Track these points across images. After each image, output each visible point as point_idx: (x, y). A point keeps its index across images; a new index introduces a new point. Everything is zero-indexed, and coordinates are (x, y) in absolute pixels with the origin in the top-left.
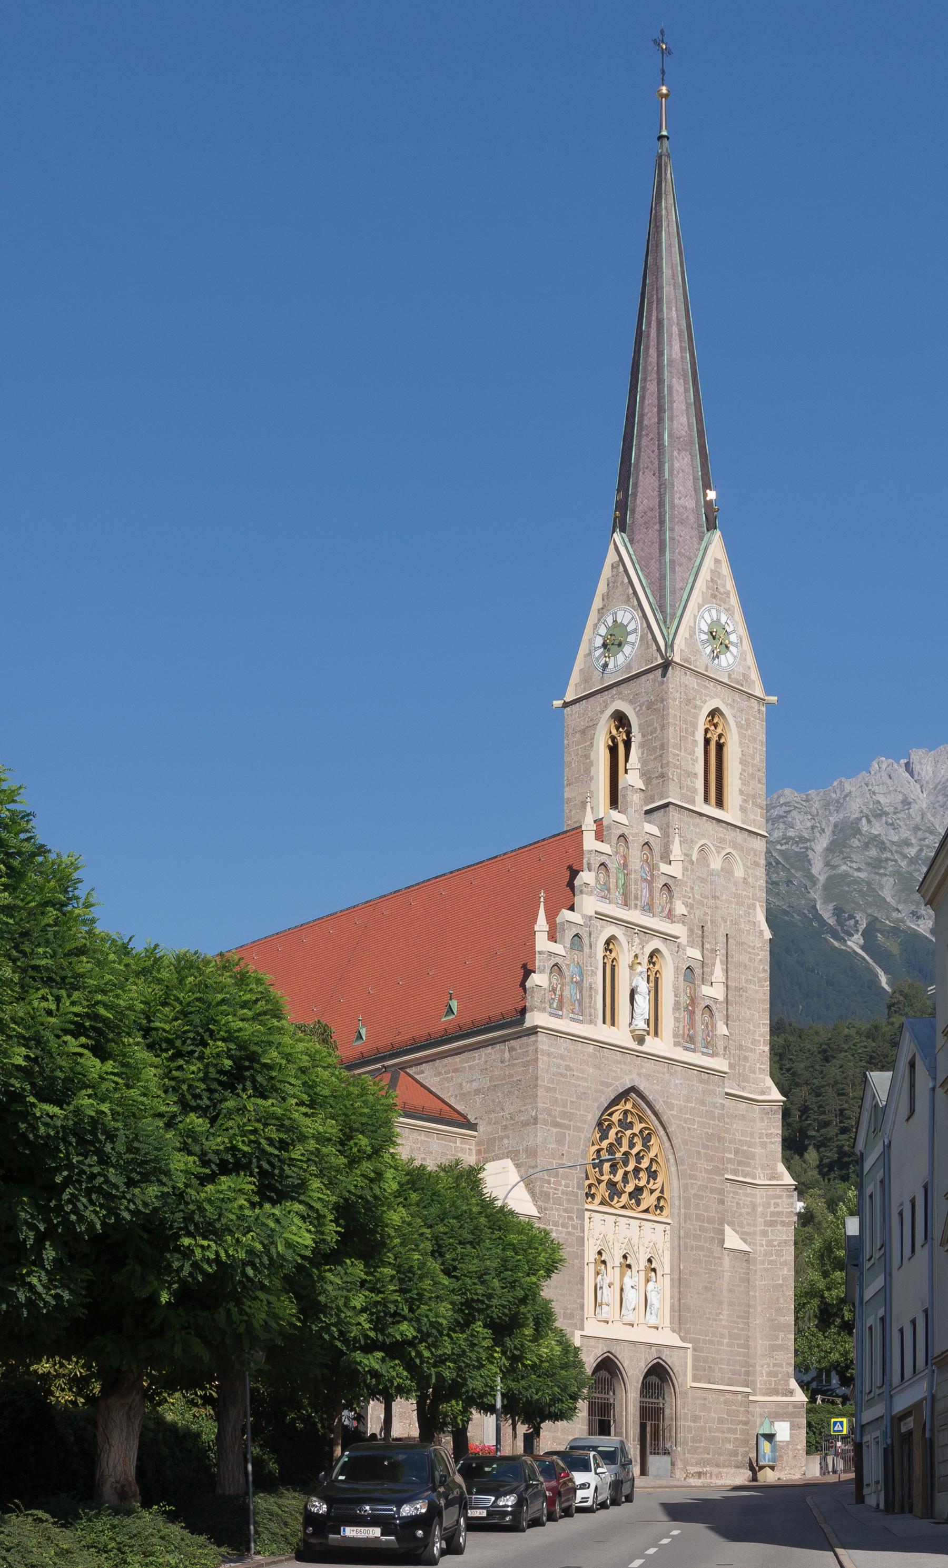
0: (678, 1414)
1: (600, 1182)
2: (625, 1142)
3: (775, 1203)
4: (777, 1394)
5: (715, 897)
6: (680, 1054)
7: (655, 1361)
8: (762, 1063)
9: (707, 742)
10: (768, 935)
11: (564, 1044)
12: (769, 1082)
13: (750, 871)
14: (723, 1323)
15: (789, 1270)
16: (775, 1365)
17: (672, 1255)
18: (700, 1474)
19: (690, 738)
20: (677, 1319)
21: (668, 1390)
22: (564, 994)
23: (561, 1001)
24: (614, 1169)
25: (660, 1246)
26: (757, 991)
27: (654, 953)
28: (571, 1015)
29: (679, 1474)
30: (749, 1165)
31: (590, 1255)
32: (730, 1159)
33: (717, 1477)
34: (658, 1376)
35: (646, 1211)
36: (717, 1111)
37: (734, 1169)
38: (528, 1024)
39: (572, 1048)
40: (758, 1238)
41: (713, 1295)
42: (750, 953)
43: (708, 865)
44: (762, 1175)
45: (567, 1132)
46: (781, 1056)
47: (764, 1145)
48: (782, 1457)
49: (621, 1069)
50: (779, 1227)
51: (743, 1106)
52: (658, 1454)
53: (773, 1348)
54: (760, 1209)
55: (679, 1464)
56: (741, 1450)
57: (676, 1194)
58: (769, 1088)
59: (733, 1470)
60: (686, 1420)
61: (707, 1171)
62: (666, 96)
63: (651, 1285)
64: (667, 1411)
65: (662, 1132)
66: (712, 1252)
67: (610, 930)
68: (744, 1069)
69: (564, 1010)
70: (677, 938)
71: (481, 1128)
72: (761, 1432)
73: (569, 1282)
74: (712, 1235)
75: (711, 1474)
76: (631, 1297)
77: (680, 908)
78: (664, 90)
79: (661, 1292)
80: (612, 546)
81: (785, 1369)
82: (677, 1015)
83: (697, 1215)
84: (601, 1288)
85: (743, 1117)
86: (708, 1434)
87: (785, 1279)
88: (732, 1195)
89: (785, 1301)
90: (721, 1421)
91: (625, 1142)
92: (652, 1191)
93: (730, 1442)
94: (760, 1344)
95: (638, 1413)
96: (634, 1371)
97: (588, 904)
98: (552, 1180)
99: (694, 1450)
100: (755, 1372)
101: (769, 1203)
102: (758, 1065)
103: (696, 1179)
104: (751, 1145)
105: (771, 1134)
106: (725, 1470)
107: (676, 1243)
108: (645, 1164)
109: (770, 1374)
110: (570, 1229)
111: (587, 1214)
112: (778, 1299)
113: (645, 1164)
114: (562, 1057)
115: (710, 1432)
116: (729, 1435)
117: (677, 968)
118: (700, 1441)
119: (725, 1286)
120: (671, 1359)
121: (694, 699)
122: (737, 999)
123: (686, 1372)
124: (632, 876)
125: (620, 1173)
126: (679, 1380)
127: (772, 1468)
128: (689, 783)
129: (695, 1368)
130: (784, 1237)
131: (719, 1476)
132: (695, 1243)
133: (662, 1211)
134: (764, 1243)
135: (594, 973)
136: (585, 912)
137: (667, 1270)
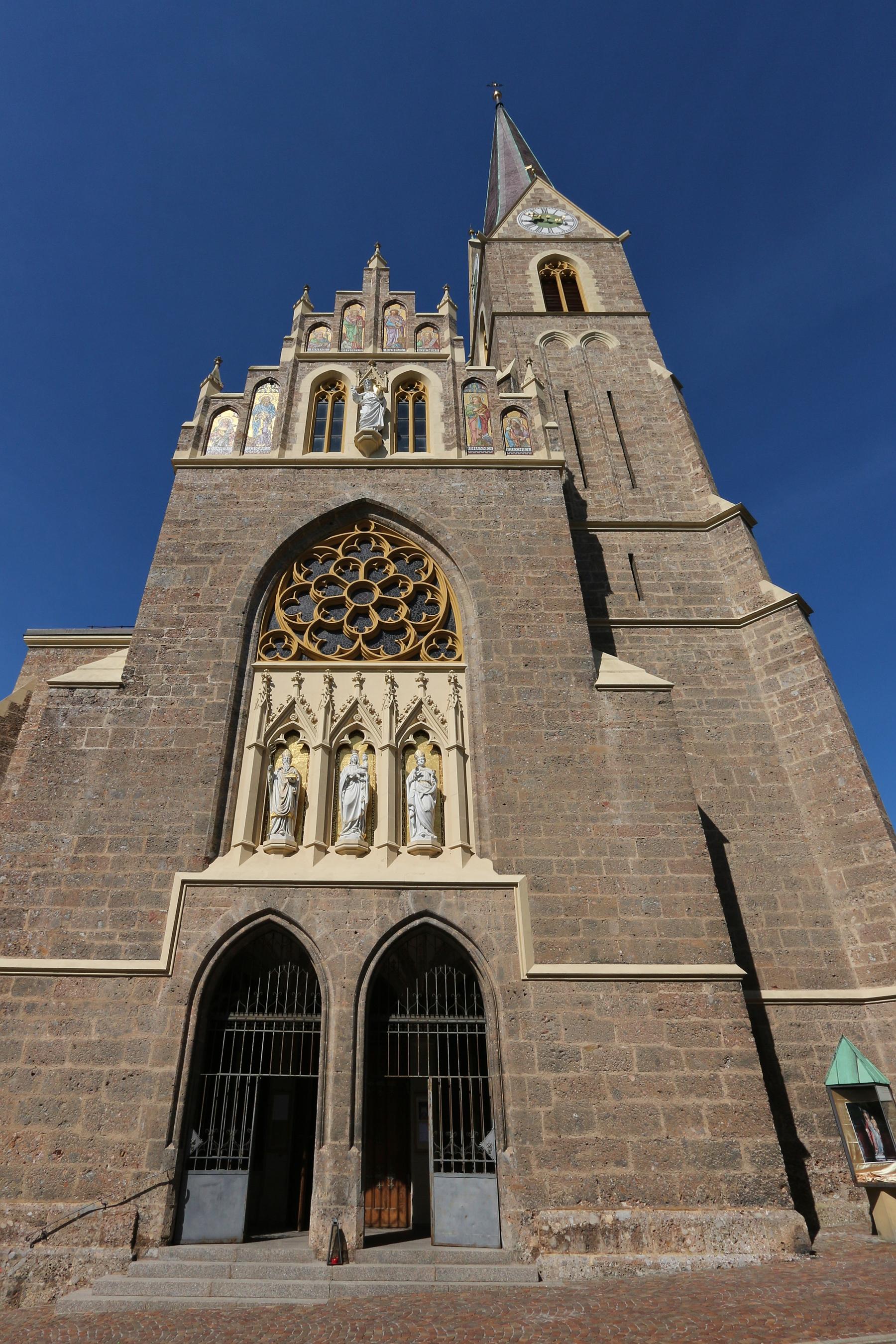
3: (772, 637)
6: (453, 455)
10: (667, 374)
14: (618, 822)
15: (835, 727)
16: (873, 913)
18: (589, 1236)
33: (664, 1244)
40: (763, 695)
44: (740, 609)
47: (731, 571)
50: (792, 667)
54: (752, 654)
59: (725, 1215)
65: (434, 549)
74: (559, 669)
75: (636, 1233)
85: (680, 548)
86: (610, 1101)
87: (833, 743)
88: (681, 642)
89: (848, 781)
90: (654, 1060)
93: (698, 1121)
99: (566, 1154)
100: (833, 937)
105: (736, 553)
106: (694, 1215)
109: (868, 934)
112: (832, 781)
115: (617, 1094)
116: (691, 1101)
118: (583, 1124)
129: (539, 927)
130: (807, 678)
131: (669, 1236)
134: (775, 699)
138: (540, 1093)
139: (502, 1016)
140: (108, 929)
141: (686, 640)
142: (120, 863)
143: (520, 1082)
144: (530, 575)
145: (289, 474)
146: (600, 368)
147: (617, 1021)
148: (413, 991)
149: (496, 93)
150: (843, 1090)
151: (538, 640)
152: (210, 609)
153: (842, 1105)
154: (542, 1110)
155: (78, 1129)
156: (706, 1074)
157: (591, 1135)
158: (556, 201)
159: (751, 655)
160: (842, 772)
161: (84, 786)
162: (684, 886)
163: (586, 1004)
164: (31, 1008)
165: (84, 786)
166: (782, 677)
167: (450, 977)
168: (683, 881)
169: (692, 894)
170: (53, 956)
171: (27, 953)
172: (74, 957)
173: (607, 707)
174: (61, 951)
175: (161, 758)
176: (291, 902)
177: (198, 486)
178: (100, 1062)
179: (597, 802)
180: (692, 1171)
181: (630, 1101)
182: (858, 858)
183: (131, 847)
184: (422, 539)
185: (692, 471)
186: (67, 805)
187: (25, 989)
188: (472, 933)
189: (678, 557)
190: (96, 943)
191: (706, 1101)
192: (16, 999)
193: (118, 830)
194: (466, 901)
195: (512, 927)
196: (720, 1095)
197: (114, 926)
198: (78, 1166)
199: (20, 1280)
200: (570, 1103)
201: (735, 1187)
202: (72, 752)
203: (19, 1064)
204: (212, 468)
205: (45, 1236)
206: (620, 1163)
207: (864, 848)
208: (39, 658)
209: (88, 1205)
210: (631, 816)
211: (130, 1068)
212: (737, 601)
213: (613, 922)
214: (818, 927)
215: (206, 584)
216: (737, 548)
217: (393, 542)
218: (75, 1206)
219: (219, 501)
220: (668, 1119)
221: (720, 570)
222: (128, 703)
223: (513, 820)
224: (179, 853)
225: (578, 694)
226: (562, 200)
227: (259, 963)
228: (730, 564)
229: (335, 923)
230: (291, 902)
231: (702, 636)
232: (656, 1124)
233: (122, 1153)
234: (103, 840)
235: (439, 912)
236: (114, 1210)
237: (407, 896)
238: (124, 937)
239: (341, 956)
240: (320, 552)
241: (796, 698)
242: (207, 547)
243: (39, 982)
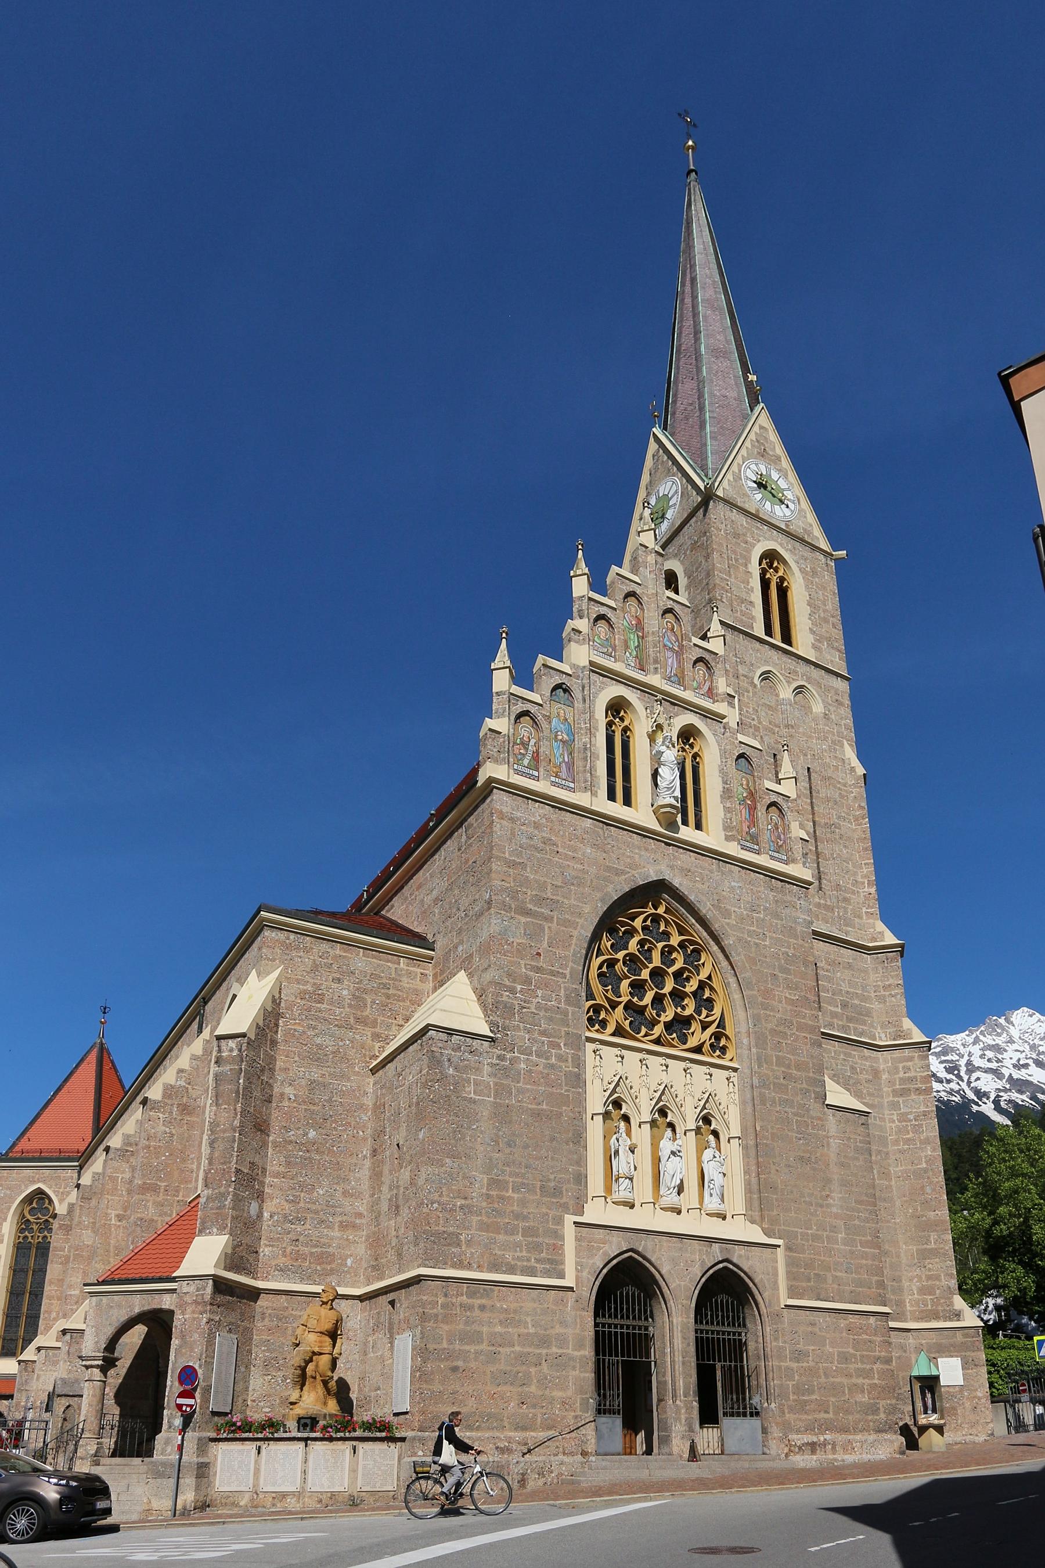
0: (768, 1349)
1: (614, 1005)
2: (656, 956)
3: (904, 1067)
4: (937, 1318)
5: (787, 726)
6: (732, 849)
7: (721, 1266)
8: (869, 907)
9: (765, 584)
10: (861, 771)
11: (539, 811)
12: (880, 926)
13: (832, 709)
14: (834, 1210)
15: (934, 1150)
16: (929, 1278)
17: (743, 1113)
18: (813, 1447)
19: (742, 568)
20: (756, 1204)
21: (751, 1316)
22: (541, 750)
23: (536, 757)
24: (638, 987)
25: (722, 1097)
26: (854, 830)
27: (688, 735)
28: (553, 779)
29: (775, 1448)
30: (864, 1023)
31: (596, 1101)
32: (836, 1013)
34: (726, 1293)
35: (698, 1050)
36: (799, 929)
37: (843, 1027)
38: (481, 779)
39: (554, 817)
40: (887, 1112)
41: (814, 1169)
42: (840, 789)
43: (777, 695)
44: (883, 1036)
45: (546, 926)
46: (950, 1149)
47: (882, 999)
48: (954, 1409)
49: (641, 856)
50: (913, 1096)
51: (847, 954)
52: (745, 1415)
53: (925, 1255)
54: (885, 1076)
55: (775, 1432)
56: (882, 1403)
57: (743, 1029)
58: (881, 933)
59: (872, 1437)
60: (781, 1358)
61: (792, 1002)
62: (692, 147)
63: (708, 1154)
64: (751, 1346)
66: (808, 1110)
67: (616, 690)
68: (846, 912)
69: (541, 770)
70: (724, 717)
71: (437, 946)
72: (915, 1373)
73: (552, 1139)
74: (805, 1085)
76: (674, 1169)
77: (722, 685)
78: (690, 143)
79: (728, 1166)
80: (652, 439)
81: (944, 1283)
82: (728, 805)
83: (777, 1057)
84: (617, 1152)
85: (849, 966)
86: (823, 1380)
87: (929, 1161)
88: (842, 1056)
89: (934, 1190)
90: (845, 1358)
91: (656, 956)
92: (705, 1026)
94: (906, 1250)
95: (692, 1349)
96: (681, 1280)
97: (579, 654)
98: (519, 987)
99: (801, 1407)
100: (901, 1289)
101: (897, 1068)
102: (864, 909)
103: (772, 1010)
104: (864, 999)
105: (890, 985)
106: (858, 1437)
107: (749, 1096)
108: (691, 986)
109: (922, 1291)
110: (553, 1060)
111: (590, 1047)
113: (691, 986)
114: (537, 826)
115: (826, 1375)
116: (860, 1381)
117: (724, 753)
118: (810, 1391)
119: (833, 1157)
120: (746, 1261)
121: (744, 535)
122: (828, 835)
123: (776, 1283)
124: (650, 639)
125: (649, 997)
126: (766, 1295)
127: (940, 1429)
128: (743, 608)
129: (791, 1276)
130: (922, 1108)
131: (848, 1447)
132: (777, 1096)
133: (724, 1053)
135: (591, 732)
136: (573, 661)
137: (735, 1131)
138: (789, 1373)
139: (768, 1329)
140: (524, 1254)
141: (845, 1054)
142: (523, 1203)
143: (780, 1367)
144: (787, 995)
145: (599, 828)
146: (804, 734)
147: (828, 1336)
148: (706, 1309)
149: (690, 143)
150: (919, 1378)
151: (792, 1057)
152: (552, 973)
153: (917, 1386)
154: (790, 1383)
155: (533, 1389)
156: (868, 1367)
157: (814, 1397)
158: (779, 458)
159: (884, 1077)
160: (931, 1183)
161: (482, 1132)
162: (864, 1256)
163: (813, 1324)
164: (482, 1308)
165: (482, 1132)
166: (904, 1102)
167: (727, 1301)
168: (866, 1253)
169: (870, 1262)
170: (490, 1271)
171: (469, 1267)
172: (505, 1273)
173: (832, 1120)
174: (494, 1267)
175: (537, 1115)
176: (646, 1245)
177: (519, 819)
178: (538, 1346)
179: (823, 1193)
180: (858, 1416)
181: (832, 1380)
182: (928, 1242)
183: (529, 1190)
184: (705, 934)
185: (866, 889)
186: (471, 1148)
187: (475, 1293)
188: (753, 1276)
189: (847, 974)
190: (519, 1263)
191: (867, 1381)
192: (470, 1301)
193: (517, 1175)
194: (750, 1254)
195: (776, 1274)
196: (873, 1378)
197: (529, 1252)
198: (539, 1411)
199: (523, 1474)
200: (805, 1379)
201: (877, 1424)
202: (465, 1099)
203: (484, 1346)
204: (528, 798)
205: (529, 1451)
206: (827, 1412)
207: (933, 1236)
208: (283, 943)
209: (551, 1433)
210: (841, 1206)
211: (560, 1351)
212: (882, 1028)
213: (829, 1275)
214: (894, 1283)
215: (545, 945)
216: (891, 981)
217: (682, 931)
218: (542, 1435)
219: (541, 845)
220: (849, 1389)
221: (873, 995)
222: (501, 1058)
223: (777, 1200)
224: (564, 1200)
225: (815, 1109)
226: (786, 463)
227: (626, 1285)
228: (883, 993)
229: (674, 1262)
230: (646, 1245)
231: (855, 1052)
232: (844, 1392)
233: (564, 1403)
234: (507, 1182)
235: (735, 1260)
236: (568, 1436)
237: (716, 1247)
238: (538, 1261)
239: (679, 1285)
240: (623, 924)
241: (911, 1121)
242: (540, 901)
243: (484, 1290)
